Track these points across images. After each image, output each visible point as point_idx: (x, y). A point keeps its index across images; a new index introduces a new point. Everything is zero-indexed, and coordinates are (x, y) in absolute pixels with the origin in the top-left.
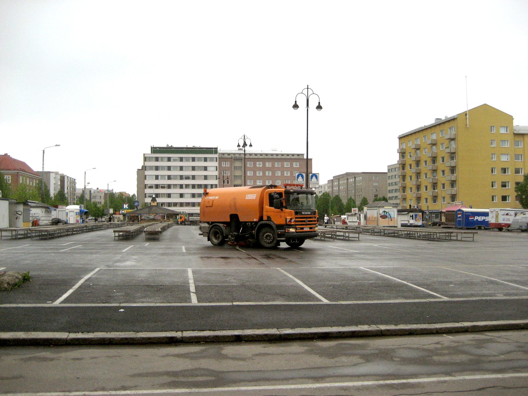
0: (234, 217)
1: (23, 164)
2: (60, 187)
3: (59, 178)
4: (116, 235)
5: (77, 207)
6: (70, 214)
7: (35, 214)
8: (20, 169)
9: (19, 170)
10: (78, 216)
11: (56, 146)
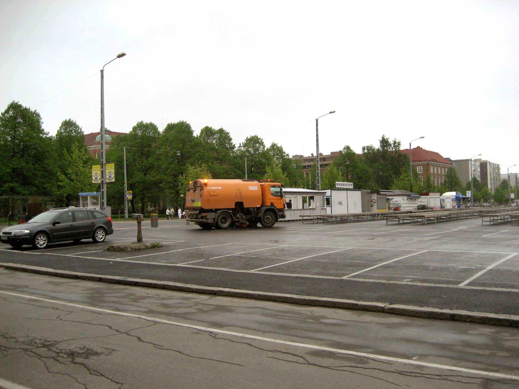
0: (240, 205)
1: (437, 154)
2: (480, 174)
3: (479, 165)
4: (491, 219)
5: (453, 194)
6: (447, 201)
7: (396, 201)
8: (431, 160)
9: (429, 161)
10: (453, 202)
11: (421, 138)
